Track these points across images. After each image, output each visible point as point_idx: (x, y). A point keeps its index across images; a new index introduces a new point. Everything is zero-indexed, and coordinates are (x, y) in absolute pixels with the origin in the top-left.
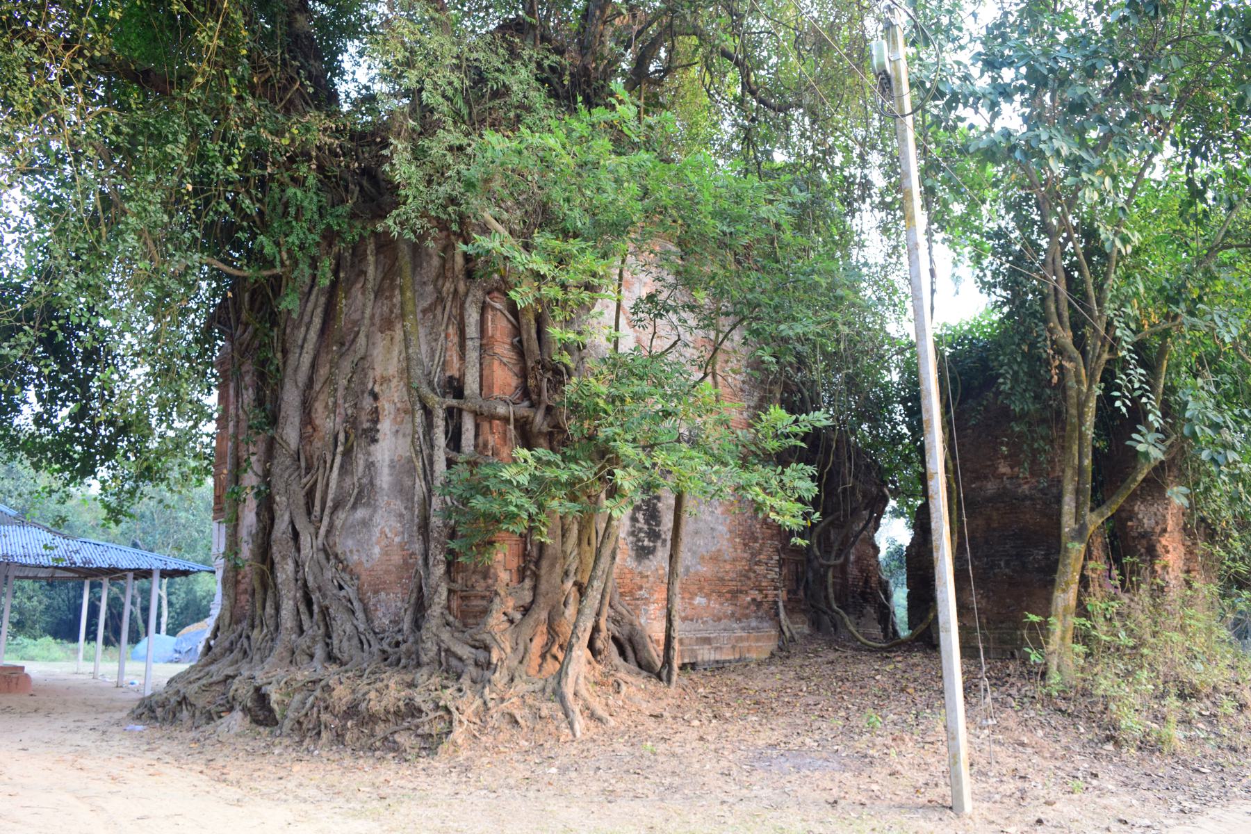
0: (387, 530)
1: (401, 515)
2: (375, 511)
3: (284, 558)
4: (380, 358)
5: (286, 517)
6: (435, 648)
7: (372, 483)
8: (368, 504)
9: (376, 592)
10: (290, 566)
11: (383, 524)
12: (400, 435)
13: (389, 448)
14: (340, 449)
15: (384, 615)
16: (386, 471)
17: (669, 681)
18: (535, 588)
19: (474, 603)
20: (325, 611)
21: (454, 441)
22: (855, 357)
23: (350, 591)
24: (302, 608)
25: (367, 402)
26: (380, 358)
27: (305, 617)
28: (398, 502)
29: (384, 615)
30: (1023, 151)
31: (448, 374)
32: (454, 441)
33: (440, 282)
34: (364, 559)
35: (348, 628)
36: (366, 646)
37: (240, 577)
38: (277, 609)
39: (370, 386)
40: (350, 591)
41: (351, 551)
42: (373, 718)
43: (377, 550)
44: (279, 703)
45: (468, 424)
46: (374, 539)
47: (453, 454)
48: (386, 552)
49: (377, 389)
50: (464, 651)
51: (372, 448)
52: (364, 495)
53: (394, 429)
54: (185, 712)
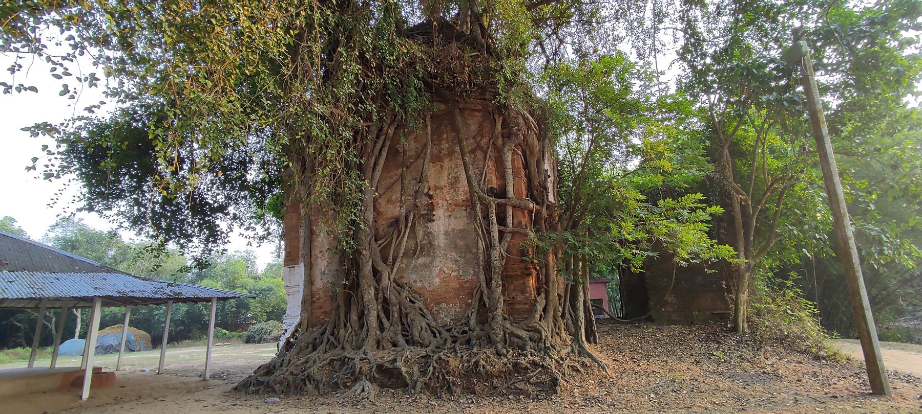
0: (445, 269)
1: (456, 261)
2: (434, 258)
4: (433, 176)
5: (370, 263)
6: (502, 333)
7: (430, 243)
8: (428, 255)
9: (438, 303)
10: (372, 291)
13: (443, 224)
15: (446, 316)
16: (442, 237)
17: (595, 342)
18: (547, 298)
19: (518, 307)
20: (403, 316)
21: (502, 221)
23: (419, 304)
24: (382, 315)
25: (424, 200)
26: (433, 176)
27: (384, 320)
28: (454, 253)
29: (446, 316)
30: (318, 101)
32: (502, 221)
33: (479, 139)
34: (426, 285)
35: (424, 325)
36: (438, 335)
39: (426, 191)
40: (419, 304)
41: (415, 281)
42: (489, 376)
43: (437, 280)
45: (510, 211)
46: (434, 274)
47: (502, 228)
48: (444, 281)
49: (431, 193)
50: (523, 334)
51: (430, 224)
52: (426, 248)
53: (447, 214)
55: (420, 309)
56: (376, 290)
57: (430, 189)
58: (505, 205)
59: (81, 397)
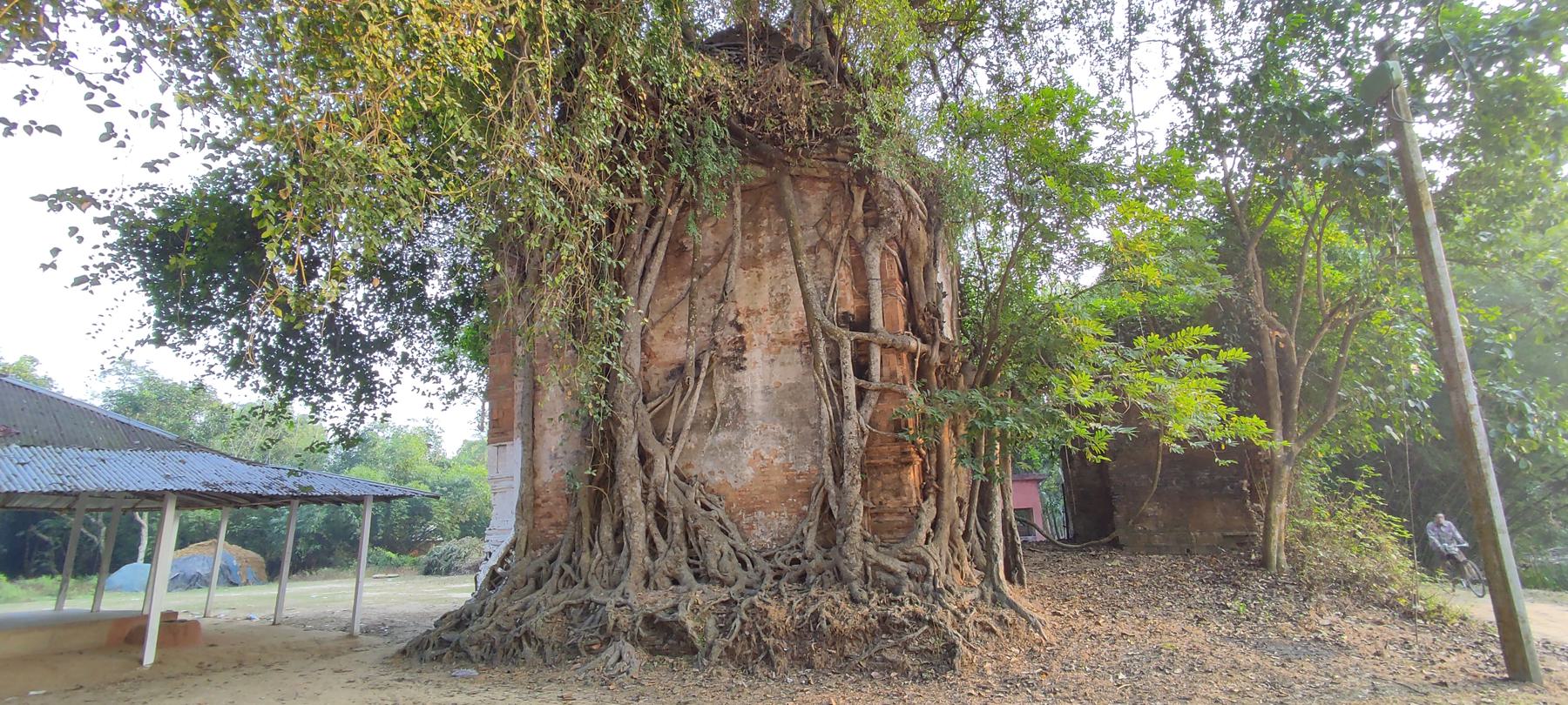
0: (763, 453)
1: (782, 438)
2: (745, 433)
3: (632, 480)
5: (635, 440)
8: (735, 428)
9: (751, 511)
10: (638, 489)
11: (757, 446)
12: (777, 364)
14: (703, 375)
15: (764, 533)
16: (758, 397)
17: (1021, 583)
18: (938, 505)
21: (862, 370)
22: (1103, 249)
23: (718, 512)
24: (655, 530)
25: (730, 333)
27: (658, 539)
29: (764, 533)
31: (842, 310)
32: (862, 370)
33: (823, 228)
34: (731, 479)
36: (749, 565)
37: (539, 501)
38: (619, 530)
40: (718, 512)
42: (838, 637)
43: (749, 472)
44: (696, 629)
45: (876, 353)
46: (744, 461)
47: (862, 382)
48: (763, 472)
49: (741, 320)
51: (738, 375)
53: (768, 358)
54: (527, 648)
55: (720, 521)
56: (645, 486)
57: (738, 314)
58: (869, 342)
59: (141, 662)
